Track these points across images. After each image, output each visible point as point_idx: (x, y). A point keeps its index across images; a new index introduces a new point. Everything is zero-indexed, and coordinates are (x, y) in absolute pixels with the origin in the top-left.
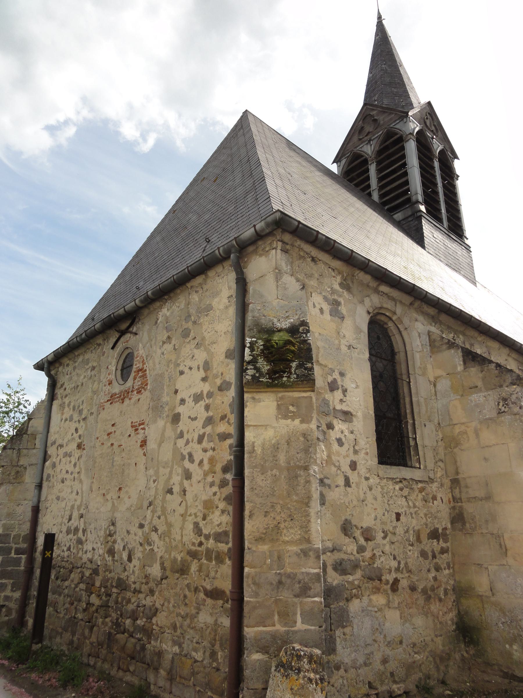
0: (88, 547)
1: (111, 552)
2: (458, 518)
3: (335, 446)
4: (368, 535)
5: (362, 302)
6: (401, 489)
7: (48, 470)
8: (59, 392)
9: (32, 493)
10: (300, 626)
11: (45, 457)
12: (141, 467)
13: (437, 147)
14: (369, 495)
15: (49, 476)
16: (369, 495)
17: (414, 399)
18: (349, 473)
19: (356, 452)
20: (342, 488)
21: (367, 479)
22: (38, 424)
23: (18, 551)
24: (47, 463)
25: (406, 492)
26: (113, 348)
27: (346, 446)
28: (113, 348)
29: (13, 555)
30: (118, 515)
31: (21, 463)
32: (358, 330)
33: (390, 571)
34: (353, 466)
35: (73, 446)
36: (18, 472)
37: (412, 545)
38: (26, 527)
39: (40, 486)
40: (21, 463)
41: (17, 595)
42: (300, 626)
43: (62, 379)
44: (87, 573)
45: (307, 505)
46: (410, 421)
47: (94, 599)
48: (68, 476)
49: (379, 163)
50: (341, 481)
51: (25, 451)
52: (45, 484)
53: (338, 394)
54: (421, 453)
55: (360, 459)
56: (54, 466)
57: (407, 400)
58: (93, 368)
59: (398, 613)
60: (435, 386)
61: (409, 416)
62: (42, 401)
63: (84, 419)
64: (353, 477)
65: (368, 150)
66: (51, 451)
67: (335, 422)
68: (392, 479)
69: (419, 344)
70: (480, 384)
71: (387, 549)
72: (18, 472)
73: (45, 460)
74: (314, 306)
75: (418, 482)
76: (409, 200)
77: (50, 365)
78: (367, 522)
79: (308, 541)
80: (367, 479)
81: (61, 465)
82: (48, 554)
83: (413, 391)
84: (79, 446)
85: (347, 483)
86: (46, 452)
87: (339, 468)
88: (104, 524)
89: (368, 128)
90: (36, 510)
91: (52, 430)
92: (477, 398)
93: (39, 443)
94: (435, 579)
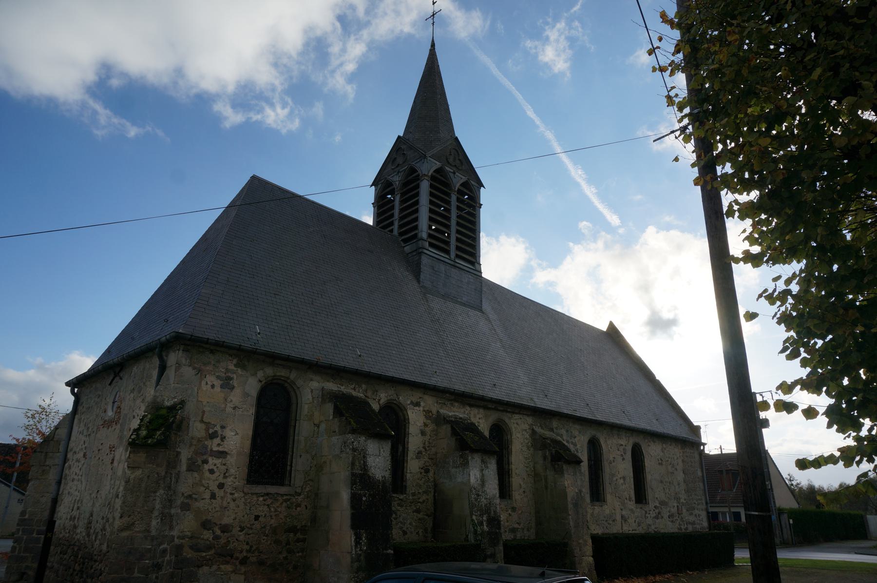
0: (78, 531)
1: (88, 535)
2: (314, 519)
3: (207, 474)
4: (225, 529)
5: (255, 374)
6: (264, 500)
7: (66, 471)
8: (80, 408)
9: (53, 488)
10: (136, 574)
11: (65, 460)
12: (109, 477)
13: (458, 180)
14: (232, 505)
15: (66, 475)
16: (232, 505)
17: (296, 438)
18: (216, 490)
19: (225, 477)
20: (208, 501)
21: (232, 494)
22: (63, 433)
23: (39, 533)
24: (66, 465)
25: (269, 502)
26: (110, 384)
27: (217, 474)
28: (110, 384)
29: (34, 535)
30: (95, 509)
31: (47, 463)
32: (246, 395)
33: (241, 552)
34: (221, 486)
35: (81, 454)
36: (44, 471)
37: (267, 536)
38: (46, 514)
39: (59, 483)
40: (47, 463)
41: (35, 565)
42: (136, 574)
43: (83, 399)
44: (76, 549)
45: (152, 512)
46: (290, 453)
47: (77, 568)
48: (76, 477)
49: (402, 195)
50: (207, 495)
51: (51, 454)
52: (63, 481)
53: (217, 441)
54: (293, 475)
55: (229, 481)
56: (70, 467)
57: (291, 438)
58: (99, 396)
59: (243, 577)
60: (318, 427)
61: (290, 450)
62: (67, 415)
63: (89, 435)
64: (220, 493)
65: (397, 180)
66: (69, 455)
67: (210, 459)
68: (256, 494)
69: (310, 398)
70: (337, 430)
71: (242, 538)
72: (44, 471)
73: (65, 462)
74: (207, 384)
75: (282, 495)
76: (415, 236)
77: (78, 384)
78: (226, 521)
79: (149, 531)
80: (232, 494)
81: (74, 469)
82: (49, 535)
83: (296, 432)
84: (85, 455)
85: (213, 496)
86: (66, 456)
87: (207, 488)
88: (87, 515)
89: (400, 160)
90: (55, 502)
91: (73, 438)
92: (334, 439)
93: (62, 448)
94: (286, 558)
